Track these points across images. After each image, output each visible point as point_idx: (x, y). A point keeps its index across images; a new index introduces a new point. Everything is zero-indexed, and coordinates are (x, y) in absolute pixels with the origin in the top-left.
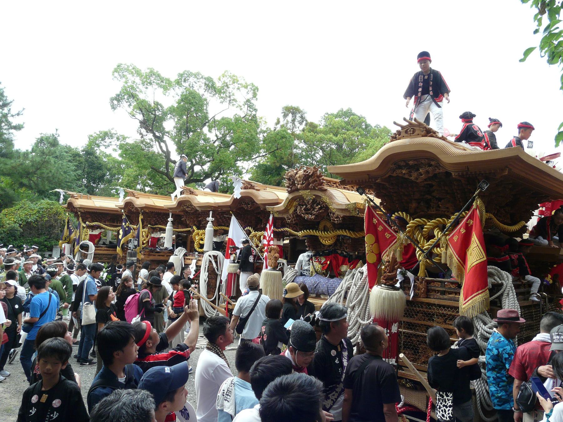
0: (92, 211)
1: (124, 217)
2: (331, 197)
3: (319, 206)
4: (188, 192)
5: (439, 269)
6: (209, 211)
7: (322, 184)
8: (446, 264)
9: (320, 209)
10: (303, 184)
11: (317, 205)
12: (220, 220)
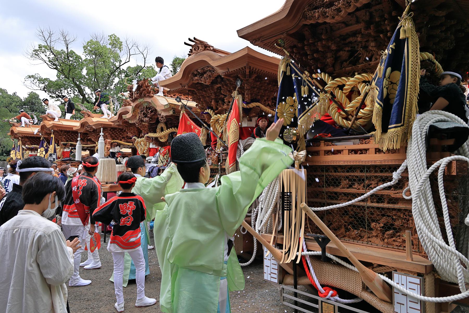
0: (29, 136)
1: (41, 139)
2: (156, 100)
6: (100, 128)
7: (150, 93)
8: (322, 79)
9: (152, 112)
10: (137, 94)
11: (149, 110)
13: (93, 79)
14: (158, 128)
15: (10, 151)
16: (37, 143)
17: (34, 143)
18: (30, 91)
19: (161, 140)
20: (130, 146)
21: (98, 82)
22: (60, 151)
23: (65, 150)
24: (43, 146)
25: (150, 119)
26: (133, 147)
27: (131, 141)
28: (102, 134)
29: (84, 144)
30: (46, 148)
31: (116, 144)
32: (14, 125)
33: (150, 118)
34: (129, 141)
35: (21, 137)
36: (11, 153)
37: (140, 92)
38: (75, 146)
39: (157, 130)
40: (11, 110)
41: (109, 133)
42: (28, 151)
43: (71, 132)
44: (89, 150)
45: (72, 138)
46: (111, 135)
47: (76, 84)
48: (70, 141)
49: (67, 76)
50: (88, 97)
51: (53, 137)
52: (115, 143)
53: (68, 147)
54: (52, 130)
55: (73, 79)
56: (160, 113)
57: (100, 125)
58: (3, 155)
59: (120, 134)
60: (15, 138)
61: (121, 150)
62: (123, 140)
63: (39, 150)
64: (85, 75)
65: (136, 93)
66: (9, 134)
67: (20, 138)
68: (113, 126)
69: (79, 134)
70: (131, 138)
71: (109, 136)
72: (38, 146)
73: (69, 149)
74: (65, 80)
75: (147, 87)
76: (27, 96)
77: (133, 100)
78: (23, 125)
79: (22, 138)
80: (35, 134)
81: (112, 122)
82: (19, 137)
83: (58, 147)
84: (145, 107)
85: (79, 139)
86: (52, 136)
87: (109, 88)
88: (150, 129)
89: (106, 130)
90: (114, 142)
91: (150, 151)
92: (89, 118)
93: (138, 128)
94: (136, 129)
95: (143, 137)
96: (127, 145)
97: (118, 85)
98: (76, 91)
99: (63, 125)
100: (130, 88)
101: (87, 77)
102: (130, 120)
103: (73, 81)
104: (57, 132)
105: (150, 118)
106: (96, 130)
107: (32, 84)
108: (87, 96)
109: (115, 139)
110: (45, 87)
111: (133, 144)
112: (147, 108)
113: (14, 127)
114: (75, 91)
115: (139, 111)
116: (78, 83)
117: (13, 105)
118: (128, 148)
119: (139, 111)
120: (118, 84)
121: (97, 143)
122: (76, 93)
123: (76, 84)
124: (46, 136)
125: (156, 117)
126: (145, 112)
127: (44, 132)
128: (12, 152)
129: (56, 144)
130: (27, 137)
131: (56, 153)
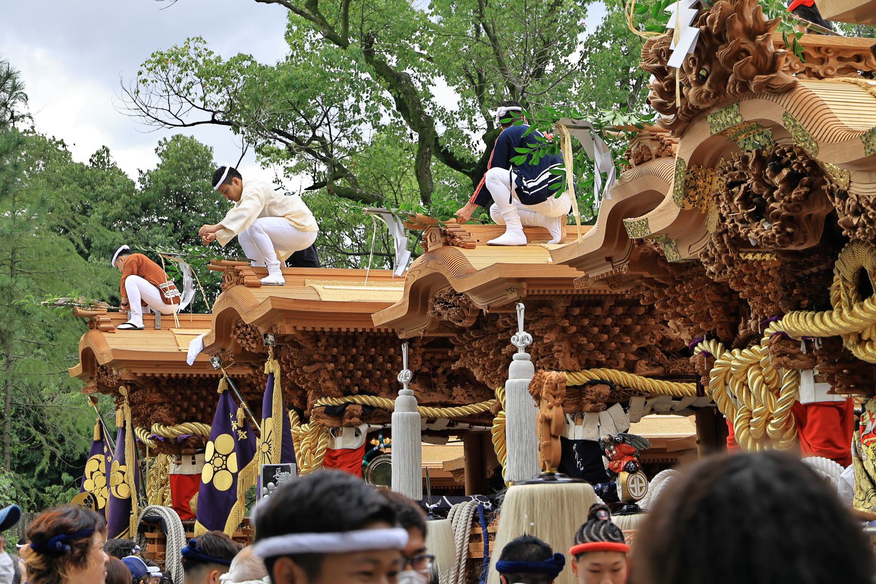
0: (165, 373)
2: (813, 107)
3: (785, 172)
4: (438, 237)
5: (240, 393)
6: (513, 305)
7: (772, 66)
9: (792, 181)
10: (700, 81)
11: (776, 171)
12: (584, 340)
13: (470, 32)
14: (837, 281)
15: (83, 461)
16: (203, 411)
17: (186, 411)
18: (169, 134)
19: (859, 353)
20: (686, 402)
21: (494, 40)
22: (312, 449)
23: (339, 443)
24: (226, 428)
25: (781, 230)
26: (702, 402)
27: (690, 372)
28: (521, 337)
29: (433, 405)
30: (242, 435)
31: (606, 390)
32: (92, 323)
33: (788, 221)
34: (677, 366)
35: (126, 384)
36: (87, 472)
37: (716, 68)
38: (385, 415)
39: (833, 294)
40: (88, 243)
41: (564, 330)
42: (161, 458)
43: (362, 341)
44: (462, 434)
45: (369, 374)
46: (571, 340)
47: (381, 70)
48: (361, 392)
49: (339, 31)
50: (449, 134)
51: (277, 375)
52: (598, 388)
53: (350, 426)
54: (271, 338)
55: (368, 41)
56: (842, 182)
57: (510, 290)
58: (59, 482)
59: (626, 330)
60: (103, 388)
61: (636, 430)
62: (642, 365)
63: (210, 446)
64: (427, 11)
65: (692, 77)
66: (77, 369)
67: (123, 390)
68: (578, 287)
69: (405, 349)
70: (687, 352)
71: (565, 345)
72: (207, 428)
73: (357, 434)
74: (325, 53)
75: (751, 33)
76: (152, 162)
77: (677, 122)
78: (137, 319)
79: (133, 386)
80: (190, 362)
81: (572, 263)
82: (121, 382)
83: (305, 427)
84: (752, 157)
85: (404, 375)
86: (272, 366)
87: (559, 67)
88: (787, 287)
89: (544, 311)
90: (593, 383)
91: (801, 424)
92: (451, 251)
93: (722, 289)
94: (709, 295)
95: (755, 338)
96: (663, 394)
97: (607, 45)
98: (388, 105)
99: (321, 302)
100: (658, 53)
101: (434, 20)
102: (668, 241)
103: (369, 54)
104: (295, 344)
105: (788, 221)
106: (493, 317)
107: (174, 98)
108: (440, 129)
109: (599, 365)
110: (231, 105)
111: (700, 392)
112: (761, 160)
113: (94, 333)
114: (382, 108)
115: (718, 183)
116: (392, 61)
117: (96, 216)
118: (672, 411)
119: (715, 186)
120: (603, 39)
121: (498, 392)
122: (386, 120)
123: (381, 70)
124: (245, 372)
125: (820, 211)
126: (754, 189)
127: (230, 348)
128: (91, 465)
129: (291, 414)
130: (155, 382)
131: (294, 461)
